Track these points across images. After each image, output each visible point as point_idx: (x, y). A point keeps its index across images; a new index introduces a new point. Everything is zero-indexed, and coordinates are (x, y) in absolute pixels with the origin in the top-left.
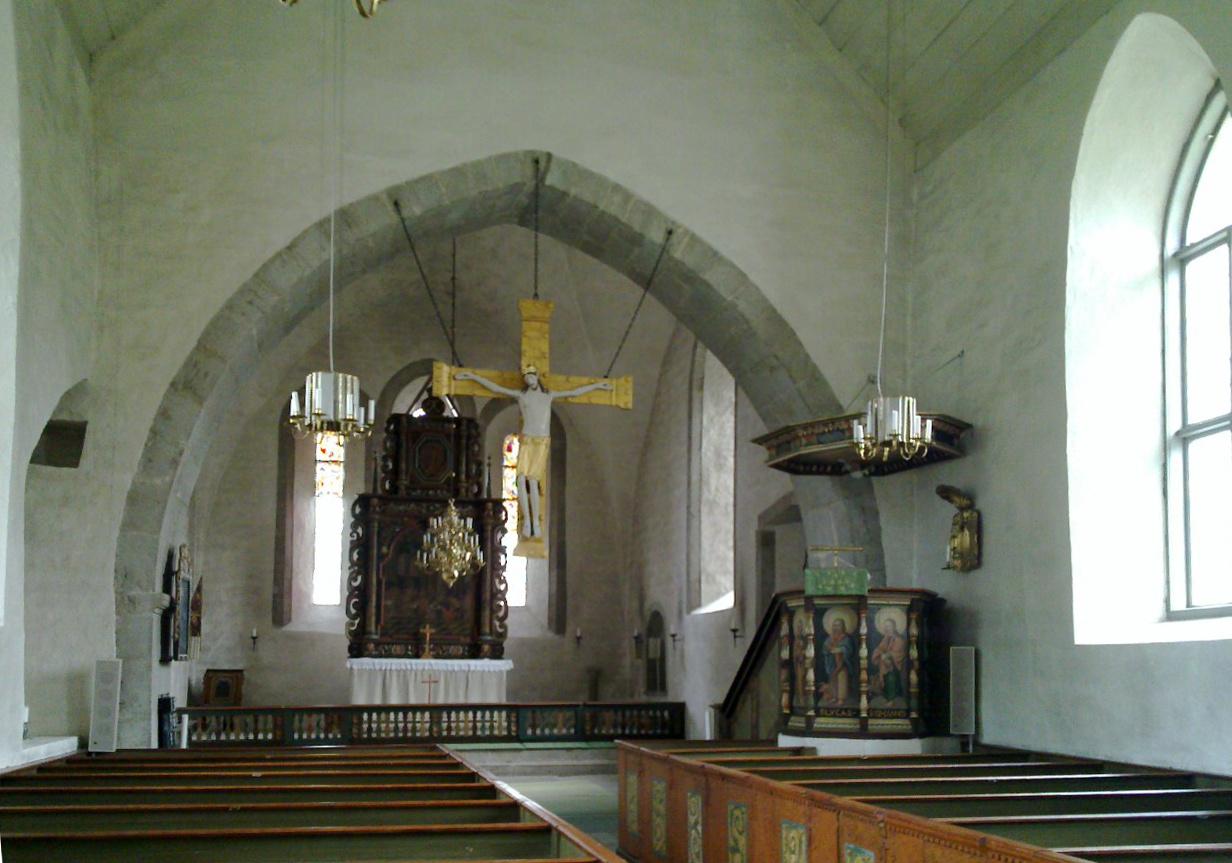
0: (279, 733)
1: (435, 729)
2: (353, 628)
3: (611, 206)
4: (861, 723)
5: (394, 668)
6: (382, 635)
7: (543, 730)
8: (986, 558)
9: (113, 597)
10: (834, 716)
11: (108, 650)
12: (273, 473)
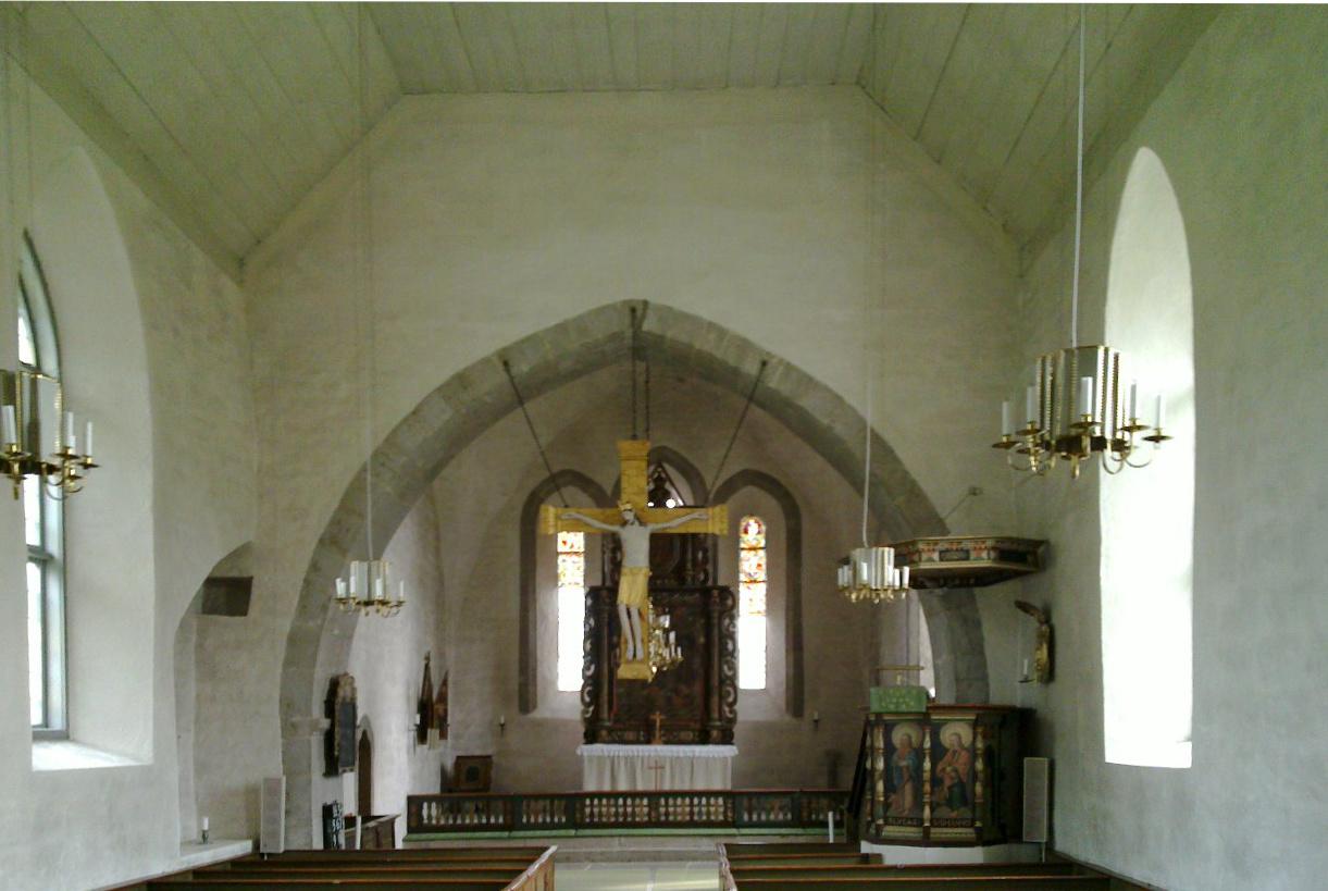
0: (509, 817)
1: (653, 814)
2: (588, 715)
3: (705, 344)
4: (924, 832)
5: (621, 754)
6: (616, 722)
7: (759, 815)
8: (1059, 670)
9: (278, 722)
10: (901, 825)
11: (274, 767)
12: (517, 569)
